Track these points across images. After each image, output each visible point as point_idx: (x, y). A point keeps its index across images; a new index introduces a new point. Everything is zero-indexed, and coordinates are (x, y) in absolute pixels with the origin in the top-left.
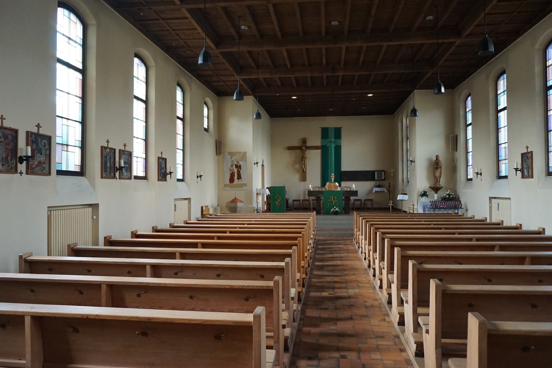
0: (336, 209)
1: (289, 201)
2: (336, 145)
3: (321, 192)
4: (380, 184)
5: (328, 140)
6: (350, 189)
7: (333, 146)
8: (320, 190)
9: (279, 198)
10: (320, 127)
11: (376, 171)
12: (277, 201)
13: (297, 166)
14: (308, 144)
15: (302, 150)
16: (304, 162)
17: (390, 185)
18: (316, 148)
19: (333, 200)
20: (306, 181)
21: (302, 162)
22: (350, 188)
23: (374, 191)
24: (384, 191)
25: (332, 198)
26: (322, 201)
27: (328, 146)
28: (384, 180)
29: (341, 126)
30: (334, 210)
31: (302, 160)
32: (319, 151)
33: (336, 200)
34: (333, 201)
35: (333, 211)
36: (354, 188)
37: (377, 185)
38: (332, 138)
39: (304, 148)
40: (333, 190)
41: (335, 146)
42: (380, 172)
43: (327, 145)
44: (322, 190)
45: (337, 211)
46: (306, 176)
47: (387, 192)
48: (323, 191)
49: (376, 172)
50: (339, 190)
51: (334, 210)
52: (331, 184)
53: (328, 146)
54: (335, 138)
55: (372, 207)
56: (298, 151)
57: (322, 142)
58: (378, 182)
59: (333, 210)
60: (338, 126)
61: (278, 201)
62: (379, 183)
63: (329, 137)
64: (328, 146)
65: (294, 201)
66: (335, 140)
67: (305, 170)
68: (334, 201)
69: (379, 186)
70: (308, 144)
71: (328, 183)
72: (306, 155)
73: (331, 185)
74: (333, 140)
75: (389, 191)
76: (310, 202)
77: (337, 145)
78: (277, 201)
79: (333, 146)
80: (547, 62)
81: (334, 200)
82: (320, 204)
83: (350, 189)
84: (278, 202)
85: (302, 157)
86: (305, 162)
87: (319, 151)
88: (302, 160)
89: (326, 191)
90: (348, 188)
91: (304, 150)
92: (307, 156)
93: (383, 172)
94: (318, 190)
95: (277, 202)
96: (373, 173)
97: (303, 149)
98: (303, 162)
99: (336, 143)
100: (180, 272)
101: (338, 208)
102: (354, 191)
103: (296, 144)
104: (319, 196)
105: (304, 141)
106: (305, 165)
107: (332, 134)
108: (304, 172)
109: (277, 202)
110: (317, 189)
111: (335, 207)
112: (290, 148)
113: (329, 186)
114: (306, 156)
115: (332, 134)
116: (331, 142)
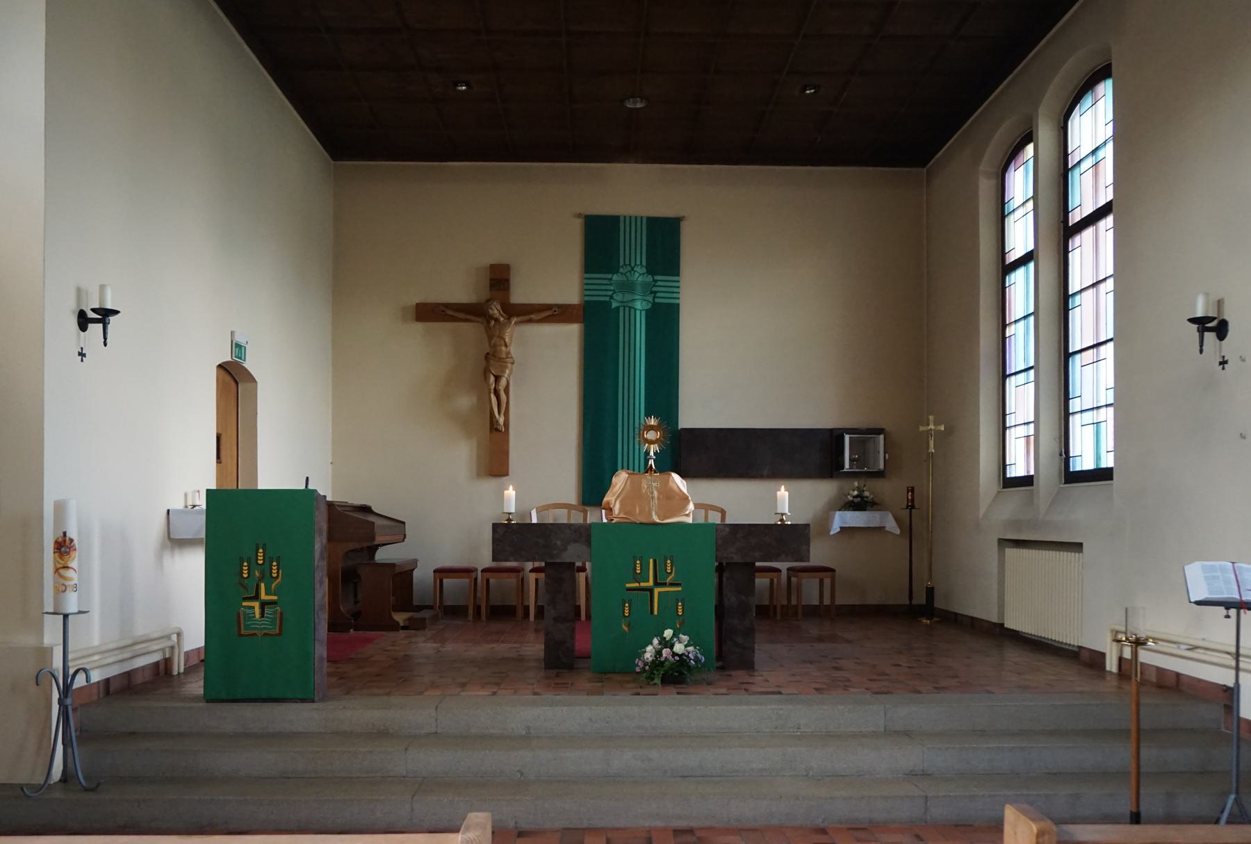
0: (679, 648)
1: (415, 573)
2: (654, 304)
3: (583, 534)
4: (867, 494)
5: (615, 277)
6: (723, 518)
7: (640, 306)
8: (577, 518)
9: (266, 576)
10: (579, 215)
11: (850, 431)
12: (256, 597)
13: (465, 402)
14: (520, 294)
15: (488, 322)
16: (497, 378)
17: (913, 500)
18: (556, 314)
19: (651, 583)
20: (507, 474)
21: (486, 379)
22: (723, 513)
23: (835, 528)
24: (880, 529)
25: (645, 568)
26: (581, 577)
27: (618, 308)
28: (879, 475)
29: (681, 214)
30: (666, 652)
31: (486, 372)
32: (572, 332)
33: (672, 585)
34: (651, 590)
35: (657, 663)
36: (787, 511)
37: (850, 498)
38: (638, 269)
39: (495, 310)
40: (658, 521)
41: (649, 306)
42: (865, 435)
43: (610, 303)
44: (585, 519)
45: (682, 659)
46: (506, 453)
47: (898, 532)
48: (590, 525)
49: (847, 437)
50: (690, 520)
51: (666, 652)
52: (644, 485)
53: (614, 305)
54: (651, 270)
55: (827, 602)
56: (470, 330)
57: (585, 287)
58: (856, 484)
59: (659, 653)
60: (662, 209)
61: (263, 596)
62: (858, 489)
63: (622, 263)
64: (614, 305)
65: (441, 573)
66: (649, 278)
67: (501, 420)
68: (657, 591)
69: (859, 505)
70: (520, 294)
71: (620, 480)
72: (506, 346)
73: (640, 487)
74: (640, 276)
75: (909, 531)
76: (522, 581)
77: (657, 300)
78: (256, 597)
79: (638, 305)
80: (1070, 254)
81: (657, 584)
82: (574, 590)
83: (723, 518)
84: (263, 605)
85: (487, 356)
86: (503, 382)
87: (572, 332)
88: (486, 372)
89: (613, 528)
90: (711, 513)
91: (497, 320)
92: (513, 350)
93: (882, 437)
94: (564, 520)
95: (256, 605)
96: (833, 438)
97: (491, 317)
98: (492, 379)
99: (655, 292)
100: (575, 541)
101: (685, 638)
102: (783, 526)
103: (460, 291)
104: (566, 557)
105: (499, 279)
106: (503, 396)
107: (634, 252)
108: (497, 430)
109: (256, 605)
110: (562, 517)
111: (668, 633)
112: (427, 313)
113: (631, 497)
114: (508, 353)
115: (634, 252)
116: (628, 287)
